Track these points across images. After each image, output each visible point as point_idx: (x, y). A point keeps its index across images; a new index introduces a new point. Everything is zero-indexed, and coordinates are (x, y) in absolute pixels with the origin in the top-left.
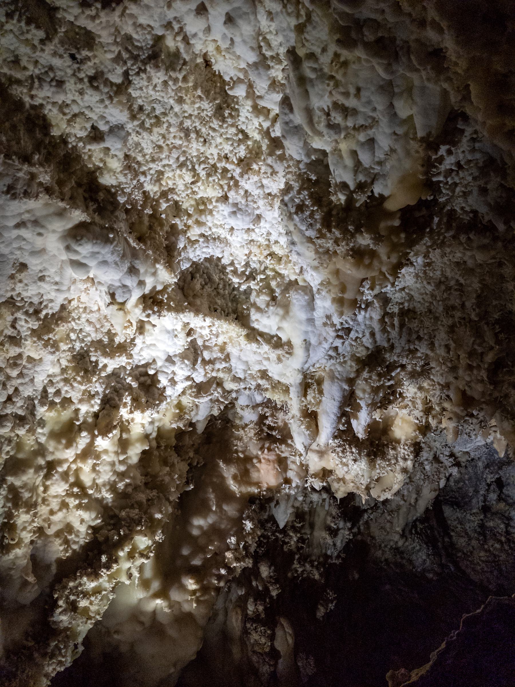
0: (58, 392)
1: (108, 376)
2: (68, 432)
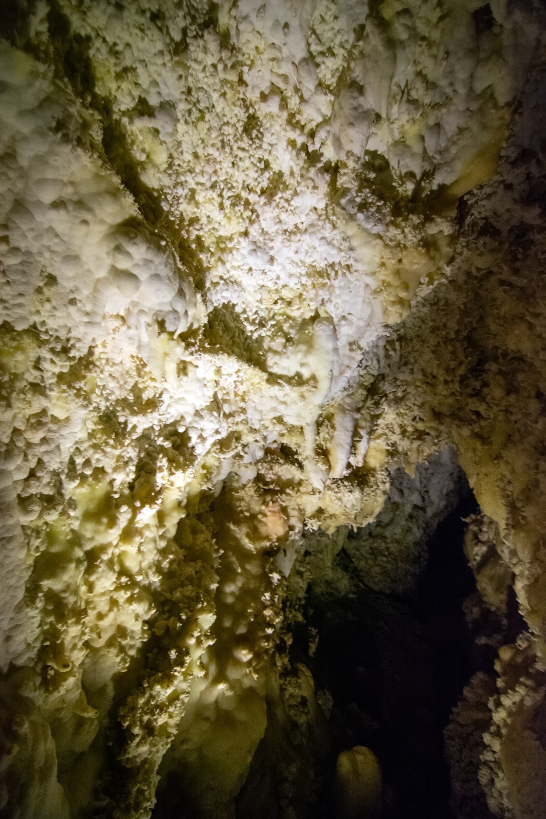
0: (87, 463)
1: (138, 439)
2: (105, 509)
